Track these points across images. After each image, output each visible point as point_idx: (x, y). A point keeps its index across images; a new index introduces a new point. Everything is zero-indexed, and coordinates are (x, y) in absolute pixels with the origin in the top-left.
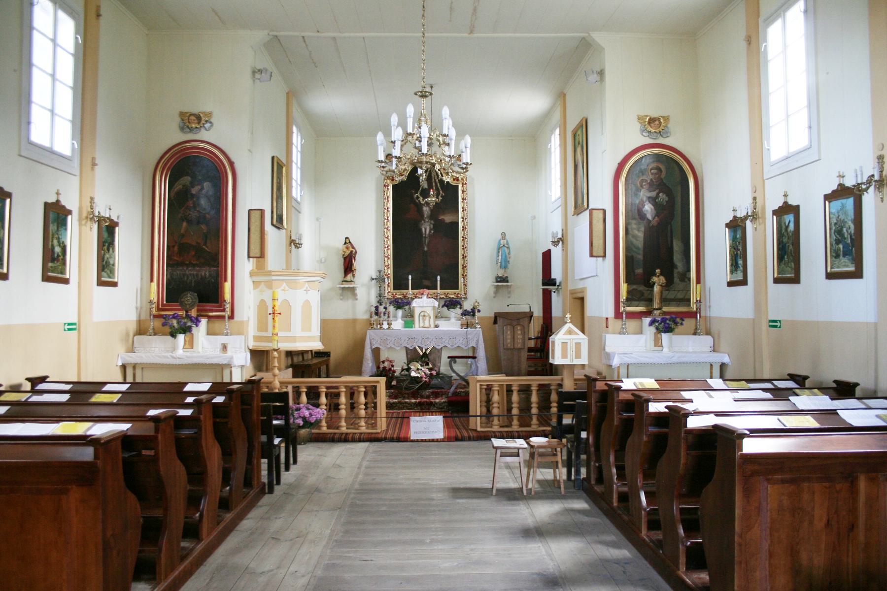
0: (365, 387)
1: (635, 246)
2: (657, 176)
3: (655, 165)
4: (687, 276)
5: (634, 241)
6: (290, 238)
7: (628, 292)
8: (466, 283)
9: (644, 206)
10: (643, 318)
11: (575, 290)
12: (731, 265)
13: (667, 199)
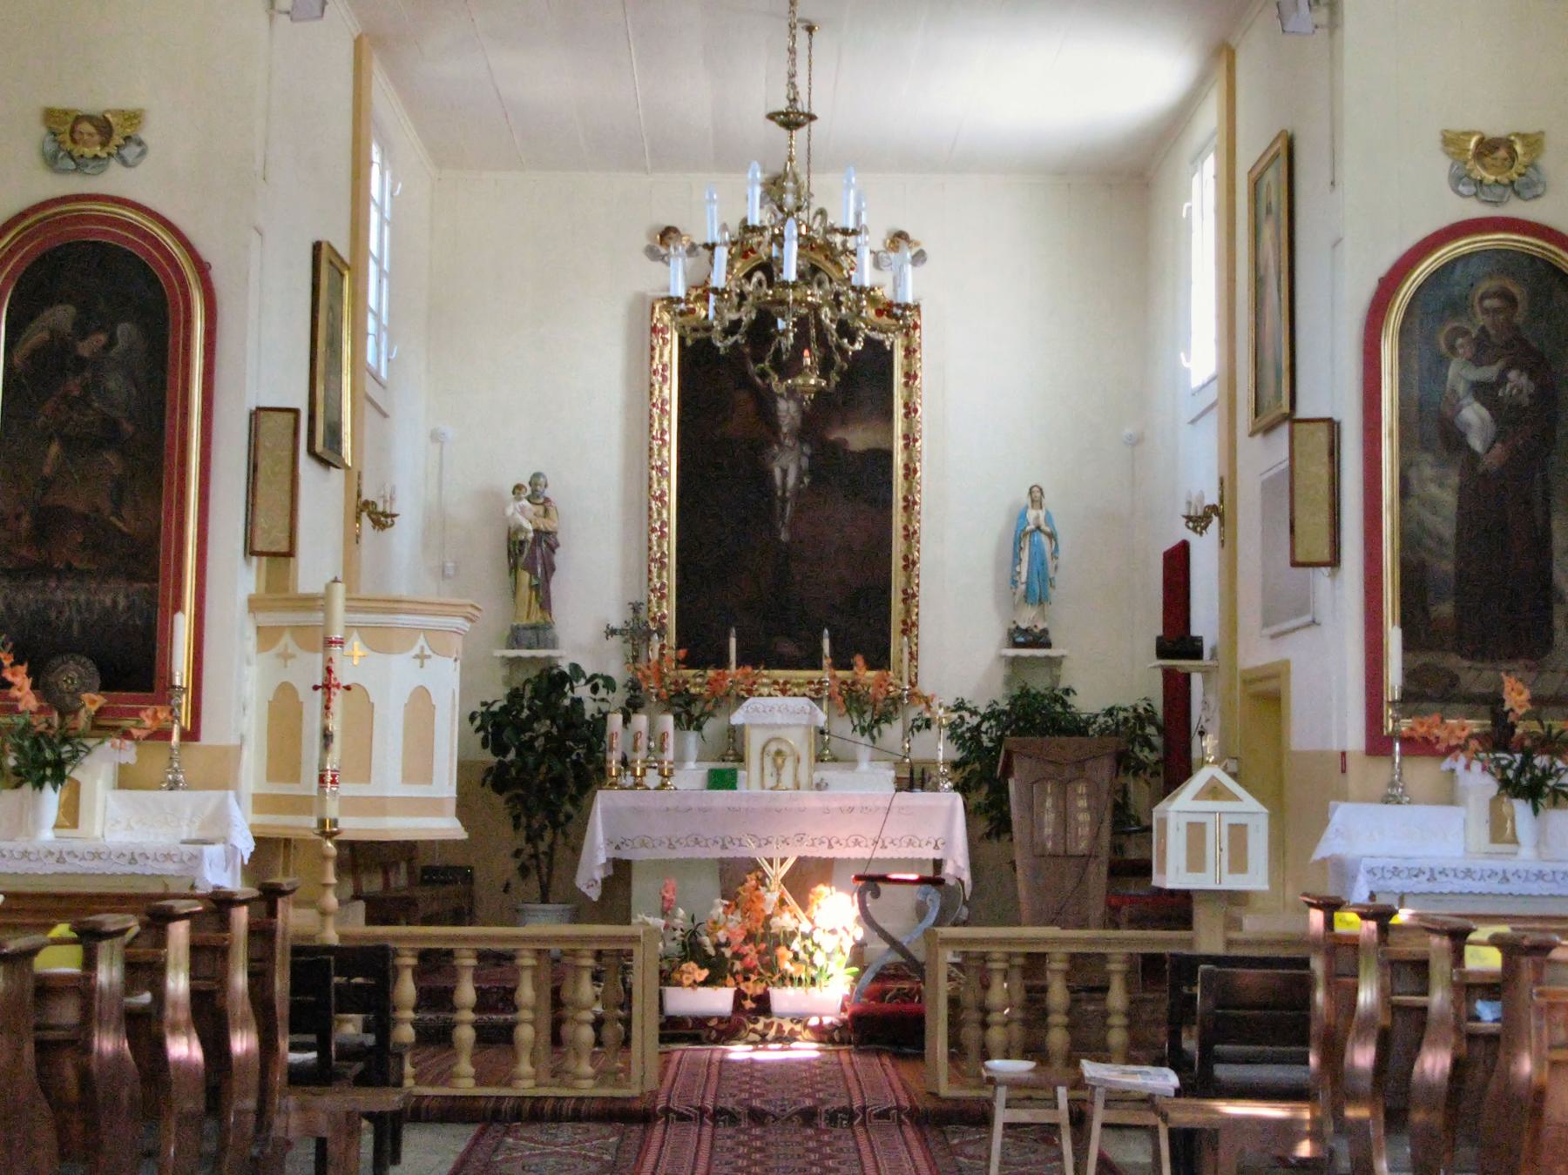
0: (599, 955)
5: (1426, 515)
6: (359, 496)
8: (914, 648)
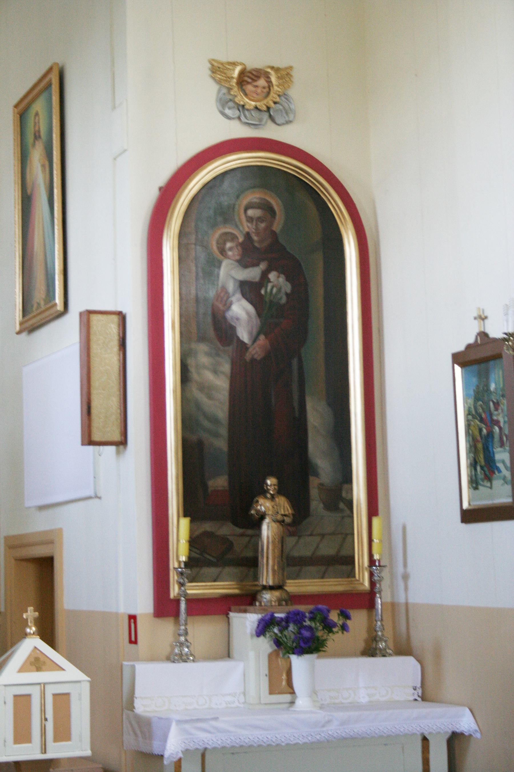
1: (206, 416)
2: (263, 225)
3: (258, 196)
4: (344, 494)
7: (193, 542)
9: (228, 307)
10: (231, 614)
11: (21, 536)
12: (473, 465)
13: (288, 288)
